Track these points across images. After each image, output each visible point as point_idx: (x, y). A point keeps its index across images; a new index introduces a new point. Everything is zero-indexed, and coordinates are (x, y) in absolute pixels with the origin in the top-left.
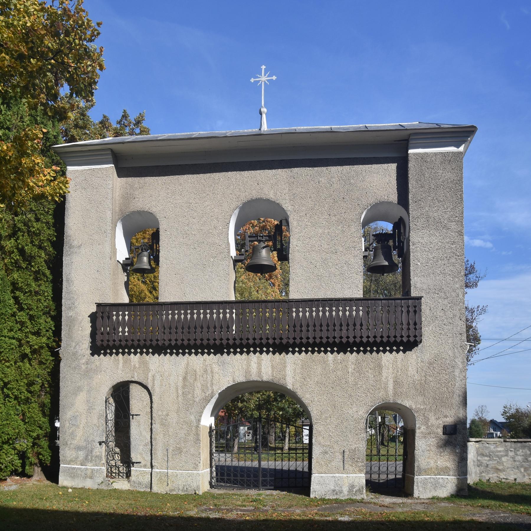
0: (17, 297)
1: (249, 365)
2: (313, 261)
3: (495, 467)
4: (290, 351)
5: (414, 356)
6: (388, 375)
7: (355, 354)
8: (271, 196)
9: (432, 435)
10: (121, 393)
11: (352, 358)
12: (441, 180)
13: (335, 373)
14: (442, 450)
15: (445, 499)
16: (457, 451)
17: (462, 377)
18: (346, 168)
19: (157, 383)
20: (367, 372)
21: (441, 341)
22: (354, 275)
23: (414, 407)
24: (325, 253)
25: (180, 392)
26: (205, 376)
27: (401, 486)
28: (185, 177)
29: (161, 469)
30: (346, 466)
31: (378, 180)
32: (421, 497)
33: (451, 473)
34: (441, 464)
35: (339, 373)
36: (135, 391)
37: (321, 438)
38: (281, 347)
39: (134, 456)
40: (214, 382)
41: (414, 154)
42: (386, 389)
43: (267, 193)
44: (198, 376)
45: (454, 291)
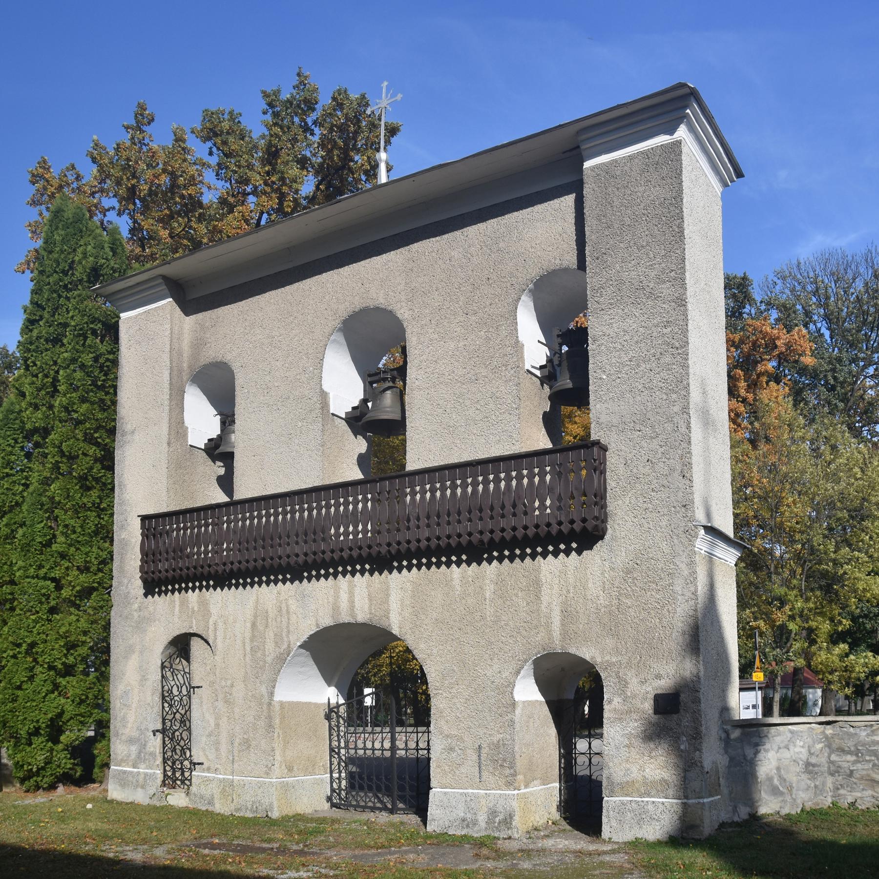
1: (337, 596)
2: (441, 402)
3: (868, 775)
4: (394, 567)
5: (597, 558)
6: (551, 599)
7: (495, 563)
9: (634, 716)
11: (490, 570)
12: (642, 205)
13: (463, 601)
14: (652, 746)
15: (659, 843)
16: (682, 747)
17: (690, 594)
18: (493, 222)
19: (220, 634)
20: (516, 595)
21: (646, 525)
22: (506, 415)
23: (599, 660)
24: (459, 384)
25: (248, 648)
26: (279, 620)
28: (267, 295)
29: (225, 774)
30: (485, 774)
31: (541, 232)
32: (615, 839)
33: (671, 792)
34: (652, 773)
35: (470, 601)
37: (443, 723)
38: (380, 560)
40: (291, 629)
41: (592, 169)
42: (548, 625)
43: (375, 296)
44: (270, 620)
45: (670, 419)
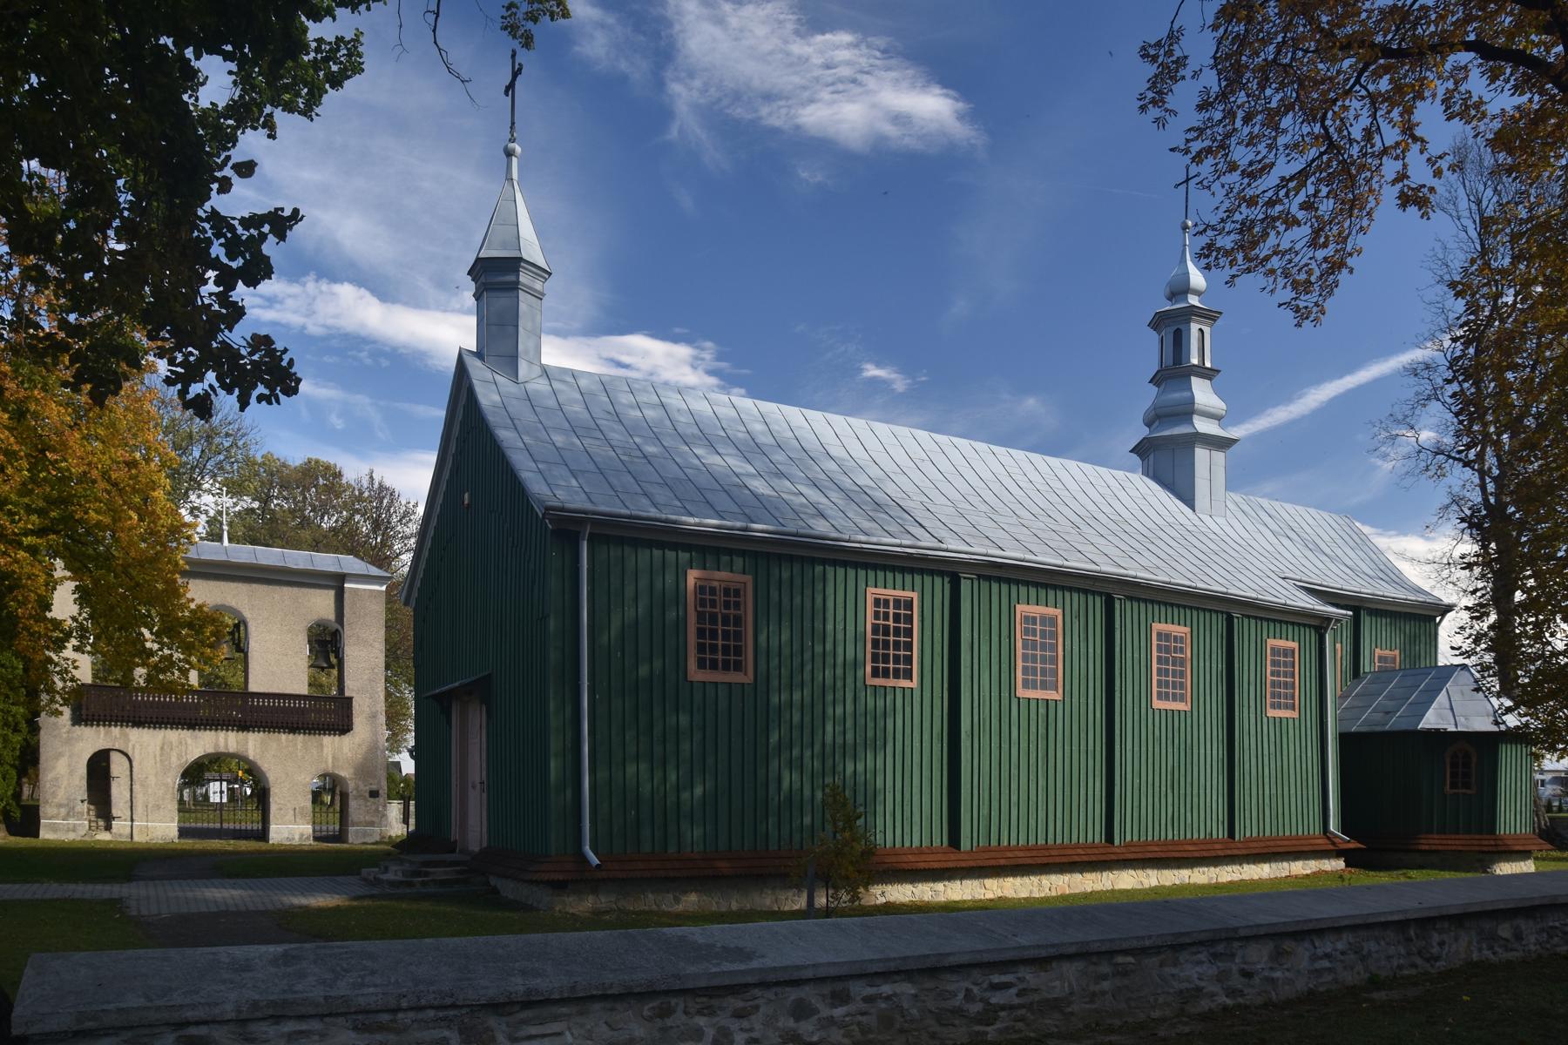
0: (196, 72)
8: (233, 604)
10: (99, 769)
27: (340, 837)
36: (116, 759)
38: (243, 727)
39: (115, 812)
